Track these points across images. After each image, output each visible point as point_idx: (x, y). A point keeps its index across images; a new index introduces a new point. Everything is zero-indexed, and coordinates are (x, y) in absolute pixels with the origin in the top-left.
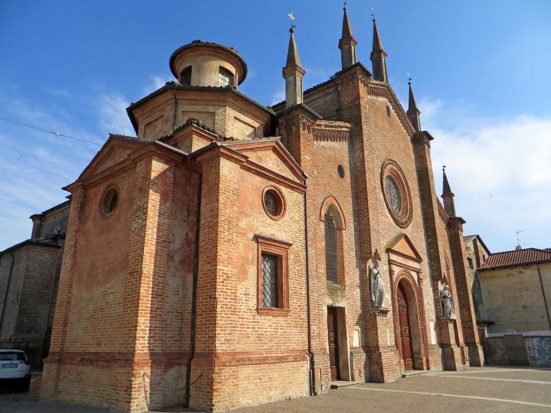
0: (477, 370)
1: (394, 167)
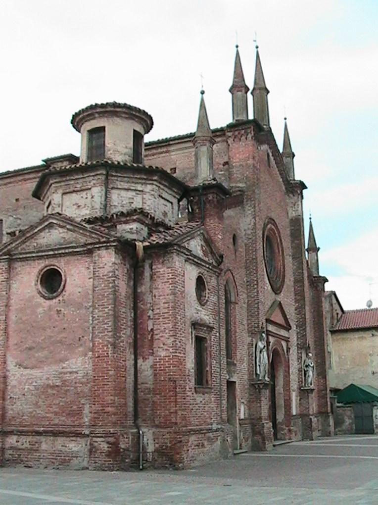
0: (327, 439)
1: (273, 227)
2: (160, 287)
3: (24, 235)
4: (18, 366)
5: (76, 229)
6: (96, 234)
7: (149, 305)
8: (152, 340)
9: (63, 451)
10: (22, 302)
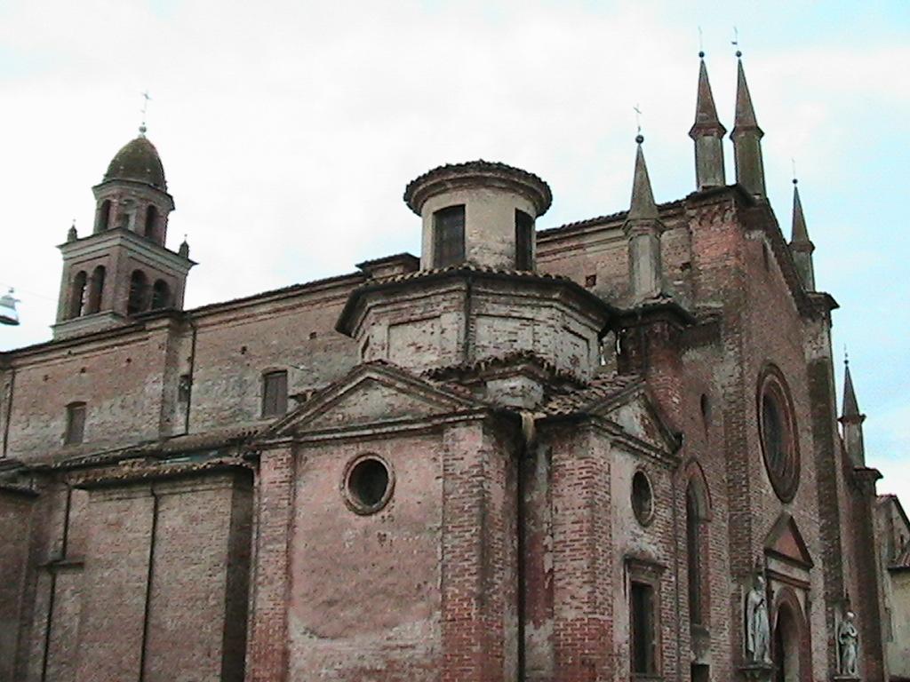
3: (320, 399)
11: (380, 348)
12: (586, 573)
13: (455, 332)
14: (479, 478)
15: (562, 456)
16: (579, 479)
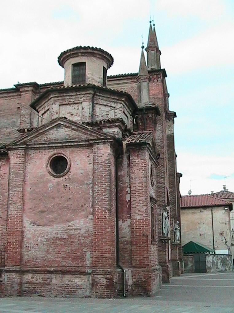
2: (135, 172)
3: (37, 131)
4: (32, 224)
5: (79, 129)
6: (95, 133)
7: (127, 184)
8: (130, 208)
9: (70, 284)
10: (36, 179)
11: (56, 113)
12: (144, 202)
13: (88, 109)
14: (108, 165)
15: (134, 158)
16: (141, 167)
